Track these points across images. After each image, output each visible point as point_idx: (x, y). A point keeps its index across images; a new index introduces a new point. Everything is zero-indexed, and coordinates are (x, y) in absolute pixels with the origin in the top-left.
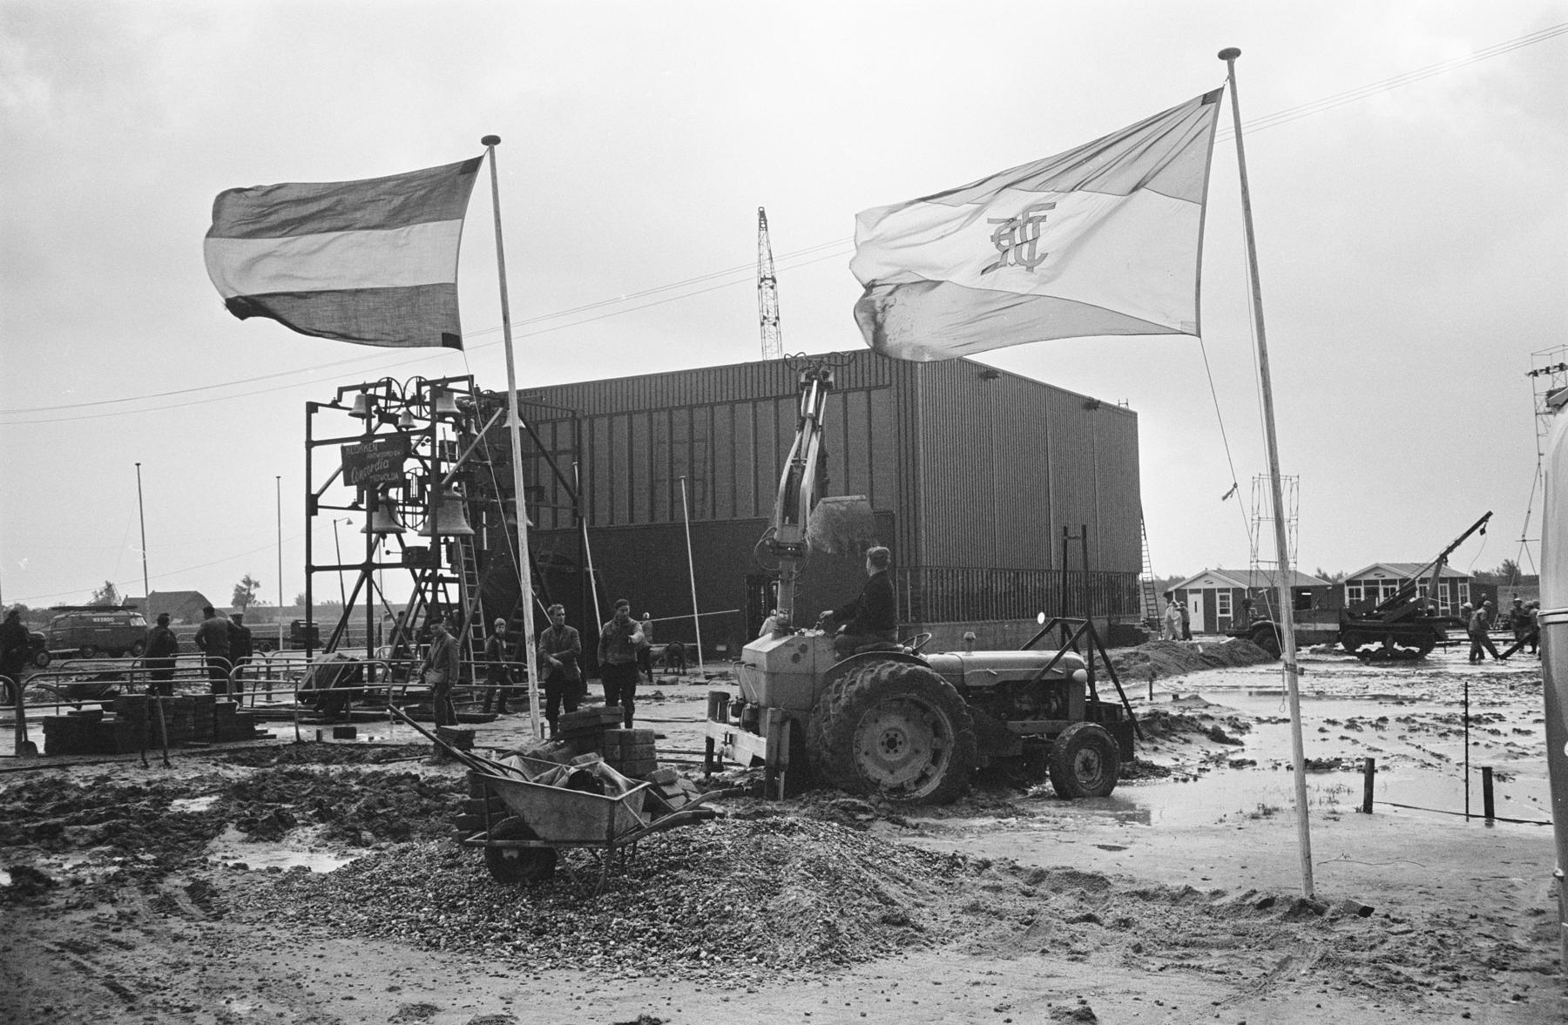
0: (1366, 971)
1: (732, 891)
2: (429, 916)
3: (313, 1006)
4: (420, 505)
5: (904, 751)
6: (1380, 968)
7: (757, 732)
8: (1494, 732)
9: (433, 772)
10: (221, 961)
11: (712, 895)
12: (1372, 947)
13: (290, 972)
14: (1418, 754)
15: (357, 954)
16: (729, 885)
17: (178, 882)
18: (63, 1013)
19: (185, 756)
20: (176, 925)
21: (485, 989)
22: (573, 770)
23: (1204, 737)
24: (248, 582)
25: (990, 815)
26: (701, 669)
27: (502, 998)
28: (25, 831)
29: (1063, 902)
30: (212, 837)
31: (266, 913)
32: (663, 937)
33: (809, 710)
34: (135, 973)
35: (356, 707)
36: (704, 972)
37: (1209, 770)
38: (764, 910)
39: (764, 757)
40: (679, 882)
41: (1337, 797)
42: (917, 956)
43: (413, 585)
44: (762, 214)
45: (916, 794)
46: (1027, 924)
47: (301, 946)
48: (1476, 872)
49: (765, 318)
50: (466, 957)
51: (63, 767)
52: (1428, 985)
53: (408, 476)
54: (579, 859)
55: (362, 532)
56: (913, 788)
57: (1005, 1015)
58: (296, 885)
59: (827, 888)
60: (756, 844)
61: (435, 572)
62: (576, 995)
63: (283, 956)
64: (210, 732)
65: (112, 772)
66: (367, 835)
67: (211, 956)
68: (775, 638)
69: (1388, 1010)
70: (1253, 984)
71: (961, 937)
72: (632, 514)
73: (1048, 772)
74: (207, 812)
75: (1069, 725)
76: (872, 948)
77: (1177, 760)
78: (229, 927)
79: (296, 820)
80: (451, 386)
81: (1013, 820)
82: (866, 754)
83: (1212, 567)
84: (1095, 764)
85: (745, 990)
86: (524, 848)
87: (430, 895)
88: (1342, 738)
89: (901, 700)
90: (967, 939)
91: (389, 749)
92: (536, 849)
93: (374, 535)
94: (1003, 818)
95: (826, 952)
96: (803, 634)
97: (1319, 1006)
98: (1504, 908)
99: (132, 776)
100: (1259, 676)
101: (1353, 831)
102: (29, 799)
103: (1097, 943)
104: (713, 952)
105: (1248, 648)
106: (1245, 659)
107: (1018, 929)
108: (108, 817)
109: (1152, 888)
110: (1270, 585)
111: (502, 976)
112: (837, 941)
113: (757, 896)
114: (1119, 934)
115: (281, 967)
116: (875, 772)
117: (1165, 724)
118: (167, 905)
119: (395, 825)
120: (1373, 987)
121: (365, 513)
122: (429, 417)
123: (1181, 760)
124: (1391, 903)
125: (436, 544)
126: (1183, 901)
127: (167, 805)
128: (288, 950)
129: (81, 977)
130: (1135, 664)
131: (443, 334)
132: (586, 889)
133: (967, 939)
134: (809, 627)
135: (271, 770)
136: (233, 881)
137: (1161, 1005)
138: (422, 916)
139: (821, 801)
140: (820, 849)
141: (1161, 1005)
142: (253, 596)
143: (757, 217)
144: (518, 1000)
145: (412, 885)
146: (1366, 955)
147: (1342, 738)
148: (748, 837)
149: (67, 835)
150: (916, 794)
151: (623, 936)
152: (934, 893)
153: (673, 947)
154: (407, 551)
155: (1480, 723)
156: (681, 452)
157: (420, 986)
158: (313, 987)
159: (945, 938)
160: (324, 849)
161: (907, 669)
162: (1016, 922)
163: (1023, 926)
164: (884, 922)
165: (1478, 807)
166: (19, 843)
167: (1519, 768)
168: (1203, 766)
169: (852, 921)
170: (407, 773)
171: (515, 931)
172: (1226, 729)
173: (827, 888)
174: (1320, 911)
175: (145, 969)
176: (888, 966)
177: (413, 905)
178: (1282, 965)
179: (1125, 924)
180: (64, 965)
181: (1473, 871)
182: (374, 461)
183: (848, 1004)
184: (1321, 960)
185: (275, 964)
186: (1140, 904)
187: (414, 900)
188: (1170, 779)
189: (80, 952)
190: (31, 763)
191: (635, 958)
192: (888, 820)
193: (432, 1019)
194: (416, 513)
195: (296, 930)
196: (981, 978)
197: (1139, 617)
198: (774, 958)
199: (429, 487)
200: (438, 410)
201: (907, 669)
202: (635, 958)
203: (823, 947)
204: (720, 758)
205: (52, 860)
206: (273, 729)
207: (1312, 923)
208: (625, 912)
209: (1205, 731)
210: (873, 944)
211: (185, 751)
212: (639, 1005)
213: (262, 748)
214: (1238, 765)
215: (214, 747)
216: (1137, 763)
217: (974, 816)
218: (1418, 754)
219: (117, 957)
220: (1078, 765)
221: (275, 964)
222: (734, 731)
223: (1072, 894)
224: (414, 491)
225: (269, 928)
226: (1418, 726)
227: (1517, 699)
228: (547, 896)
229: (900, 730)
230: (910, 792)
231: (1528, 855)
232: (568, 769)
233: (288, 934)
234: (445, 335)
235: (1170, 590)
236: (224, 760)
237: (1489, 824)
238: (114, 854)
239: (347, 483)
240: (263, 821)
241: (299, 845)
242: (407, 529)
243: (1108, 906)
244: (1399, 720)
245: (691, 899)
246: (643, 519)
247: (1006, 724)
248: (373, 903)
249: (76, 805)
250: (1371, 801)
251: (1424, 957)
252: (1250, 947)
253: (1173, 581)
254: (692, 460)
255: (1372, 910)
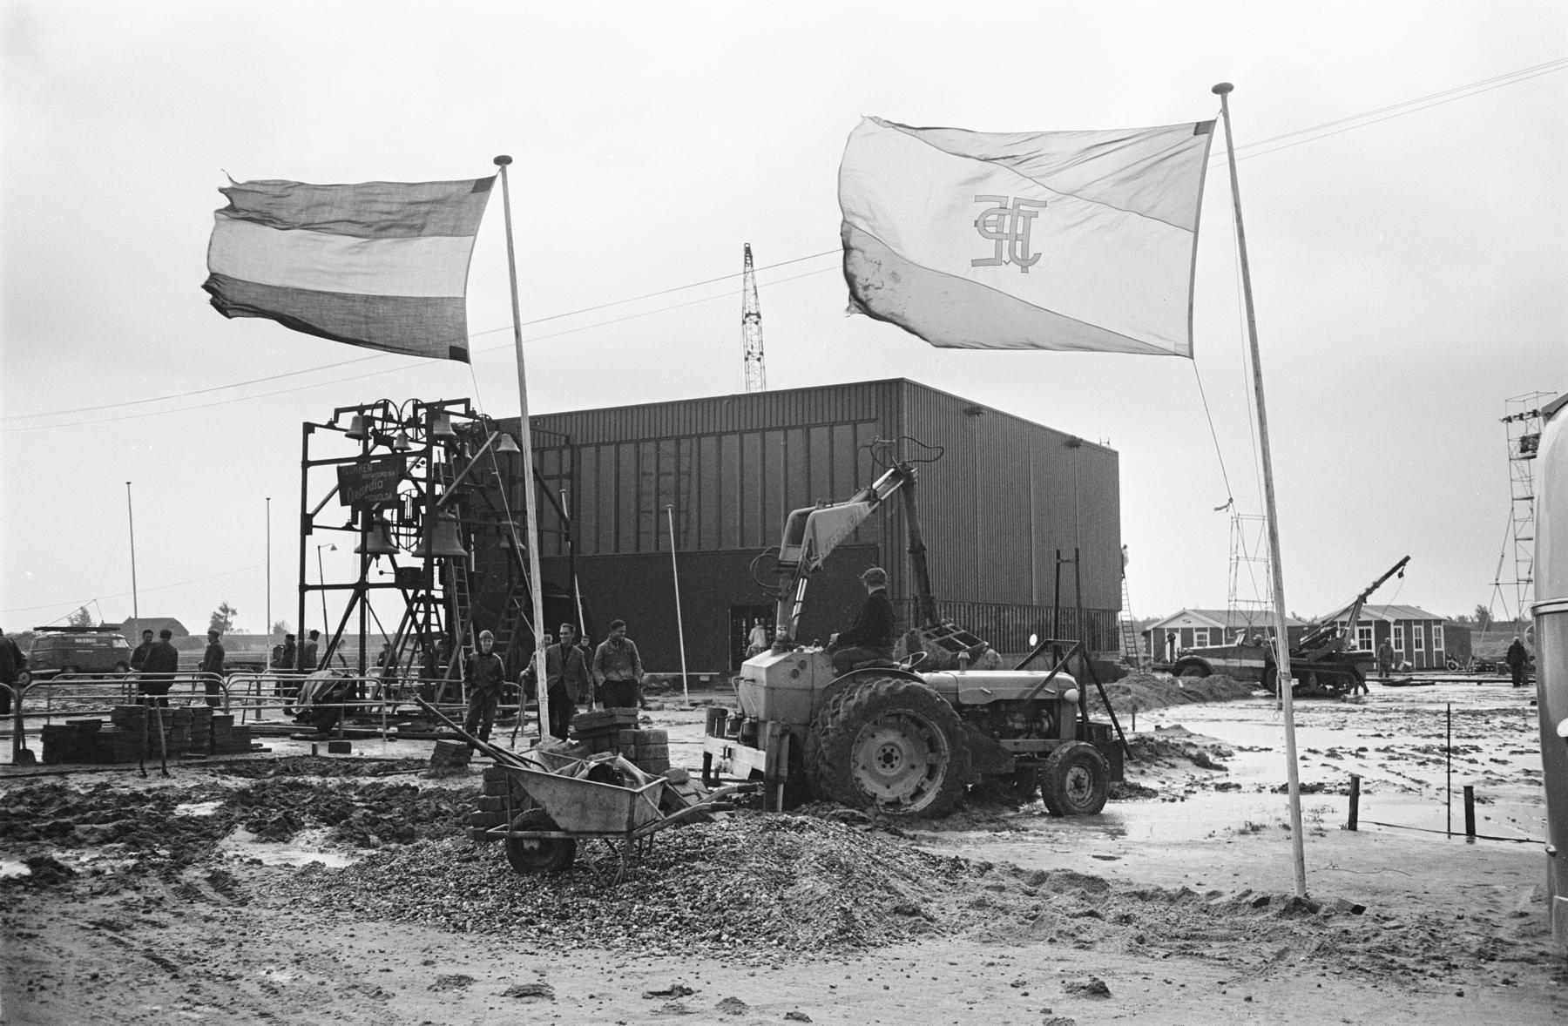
0: (1361, 959)
1: (750, 879)
2: (453, 902)
3: (352, 977)
4: (414, 527)
5: (900, 766)
6: (1375, 957)
7: (756, 746)
8: (1472, 761)
9: (430, 785)
10: (255, 939)
11: (731, 883)
12: (1366, 940)
13: (325, 949)
14: (1399, 781)
15: (386, 934)
16: (747, 875)
17: (197, 873)
18: (109, 979)
19: (183, 767)
20: (202, 908)
21: (517, 964)
22: (593, 764)
23: (1189, 763)
24: (225, 609)
25: (984, 828)
26: (686, 697)
27: (536, 971)
28: (37, 830)
29: (1067, 900)
30: (222, 837)
31: (291, 899)
32: (685, 921)
33: (807, 725)
34: (173, 947)
35: (348, 725)
36: (727, 952)
37: (1195, 792)
38: (780, 898)
39: (763, 770)
40: (697, 873)
41: (1322, 816)
42: (929, 942)
43: (405, 607)
44: (748, 251)
45: (912, 808)
46: (1032, 918)
47: (331, 927)
48: (1460, 880)
49: (749, 353)
50: (494, 937)
51: (62, 774)
52: (1421, 971)
53: (403, 498)
54: (595, 853)
55: (356, 552)
56: (909, 802)
57: (1021, 990)
58: (315, 876)
59: (840, 880)
60: (769, 839)
61: (428, 593)
62: (606, 970)
63: (314, 935)
64: (206, 744)
65: (111, 780)
66: (374, 839)
67: (244, 934)
68: (774, 654)
69: (1385, 989)
70: (1254, 969)
71: (970, 928)
72: (617, 543)
73: (1040, 793)
74: (213, 816)
75: (1061, 743)
76: (887, 935)
77: (1164, 783)
78: (256, 912)
79: (303, 823)
80: (448, 408)
81: (1007, 834)
82: (863, 768)
83: (1190, 607)
84: (1086, 782)
85: (769, 967)
86: (545, 839)
87: (451, 884)
88: (1324, 765)
89: (898, 715)
90: (976, 930)
91: (385, 763)
92: (559, 840)
93: (367, 554)
94: (997, 831)
95: (844, 936)
96: (802, 650)
97: (1319, 986)
98: (1490, 911)
99: (130, 783)
100: (1238, 711)
101: (1339, 846)
102: (31, 804)
103: (1102, 935)
104: (734, 935)
105: (1227, 683)
106: (1225, 694)
107: (1023, 923)
108: (114, 818)
109: (1150, 889)
110: (1246, 625)
111: (532, 954)
112: (853, 927)
113: (773, 886)
114: (1121, 927)
115: (314, 943)
116: (871, 786)
117: (1151, 749)
118: (190, 893)
119: (401, 830)
120: (1369, 972)
121: (360, 534)
122: (424, 440)
123: (1168, 783)
124: (1381, 905)
125: (429, 566)
126: (1180, 902)
127: (173, 809)
128: (318, 930)
129: (120, 950)
130: (1116, 696)
131: (451, 347)
132: (606, 879)
133: (976, 930)
134: (808, 645)
135: (269, 781)
136: (251, 873)
137: (1170, 983)
138: (446, 903)
139: (820, 812)
140: (832, 845)
141: (1170, 983)
142: (230, 624)
143: (743, 253)
144: (551, 974)
145: (433, 876)
146: (1360, 946)
147: (1324, 765)
148: (761, 832)
149: (77, 833)
150: (912, 808)
151: (645, 921)
152: (939, 890)
153: (695, 931)
154: (399, 572)
155: (1457, 753)
156: (668, 482)
157: (454, 961)
158: (349, 961)
159: (955, 929)
160: (333, 849)
161: (903, 685)
162: (1021, 917)
163: (1028, 921)
164: (895, 913)
165: (1459, 825)
166: (31, 839)
167: (1496, 793)
168: (1188, 788)
169: (866, 910)
170: (405, 785)
171: (539, 916)
172: (1211, 757)
173: (840, 880)
174: (1313, 909)
175: (182, 944)
176: (904, 951)
177: (435, 893)
178: (1281, 955)
179: (1126, 919)
180: (101, 940)
181: (1458, 880)
182: (369, 481)
183: (870, 980)
184: (1318, 950)
185: (308, 941)
186: (1140, 904)
187: (437, 888)
188: (1158, 799)
189: (116, 930)
190: (31, 770)
191: (659, 940)
192: (886, 830)
193: (470, 988)
194: (410, 535)
195: (322, 915)
196: (995, 961)
197: (1118, 654)
198: (794, 941)
199: (423, 509)
200: (435, 432)
201: (903, 685)
202: (659, 940)
203: (841, 932)
204: (717, 775)
205: (68, 854)
206: (266, 743)
207: (1306, 920)
208: (645, 900)
209: (1190, 757)
210: (887, 931)
211: (182, 762)
212: (670, 978)
213: (258, 760)
214: (1223, 788)
215: (211, 759)
216: (1125, 785)
217: (969, 830)
218: (1399, 781)
219: (153, 934)
220: (1069, 782)
221: (308, 941)
222: (732, 744)
223: (1074, 893)
224: (408, 512)
225: (295, 913)
226: (1397, 756)
227: (1493, 733)
228: (567, 884)
229: (897, 747)
230: (906, 805)
231: (1514, 869)
232: (587, 764)
233: (315, 918)
234: (452, 348)
235: (1148, 628)
236: (221, 772)
237: (1471, 841)
238: (127, 850)
240: (272, 823)
241: (309, 846)
242: (401, 550)
243: (1109, 905)
244: (1378, 750)
245: (710, 887)
246: (628, 548)
247: (998, 742)
248: (396, 892)
249: (78, 808)
250: (1356, 821)
251: (1417, 948)
252: (1248, 939)
253: (1149, 622)
254: (678, 489)
255: (1364, 909)
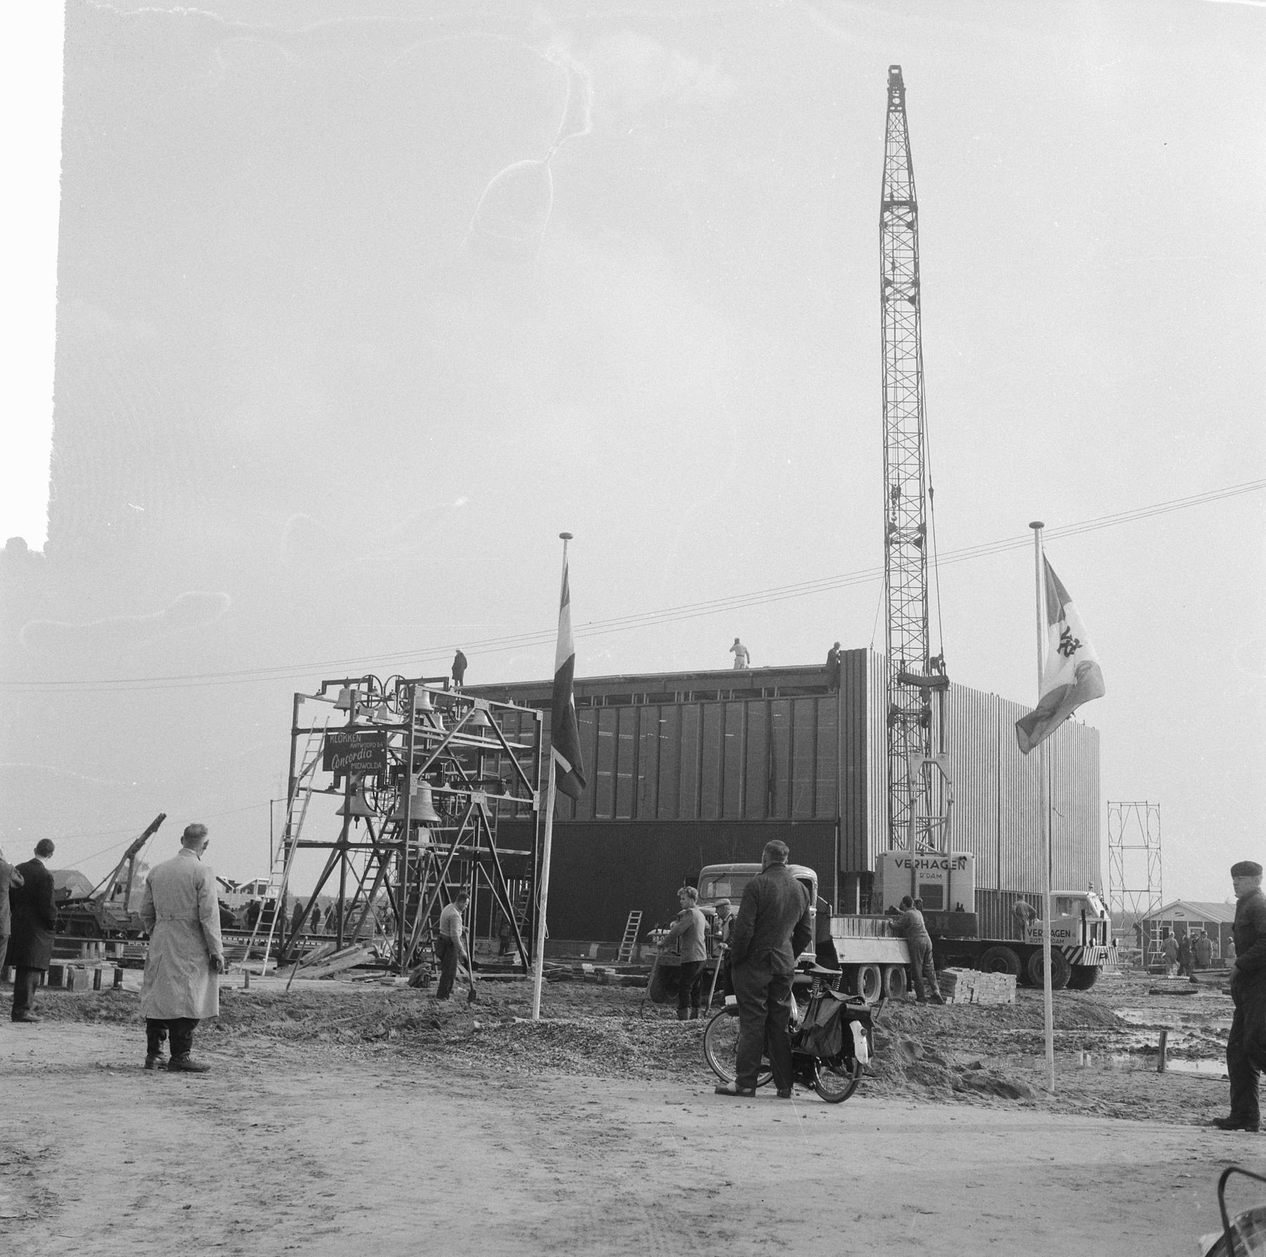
44: (896, 83)
55: (338, 814)
182: (357, 750)
239: (326, 768)
